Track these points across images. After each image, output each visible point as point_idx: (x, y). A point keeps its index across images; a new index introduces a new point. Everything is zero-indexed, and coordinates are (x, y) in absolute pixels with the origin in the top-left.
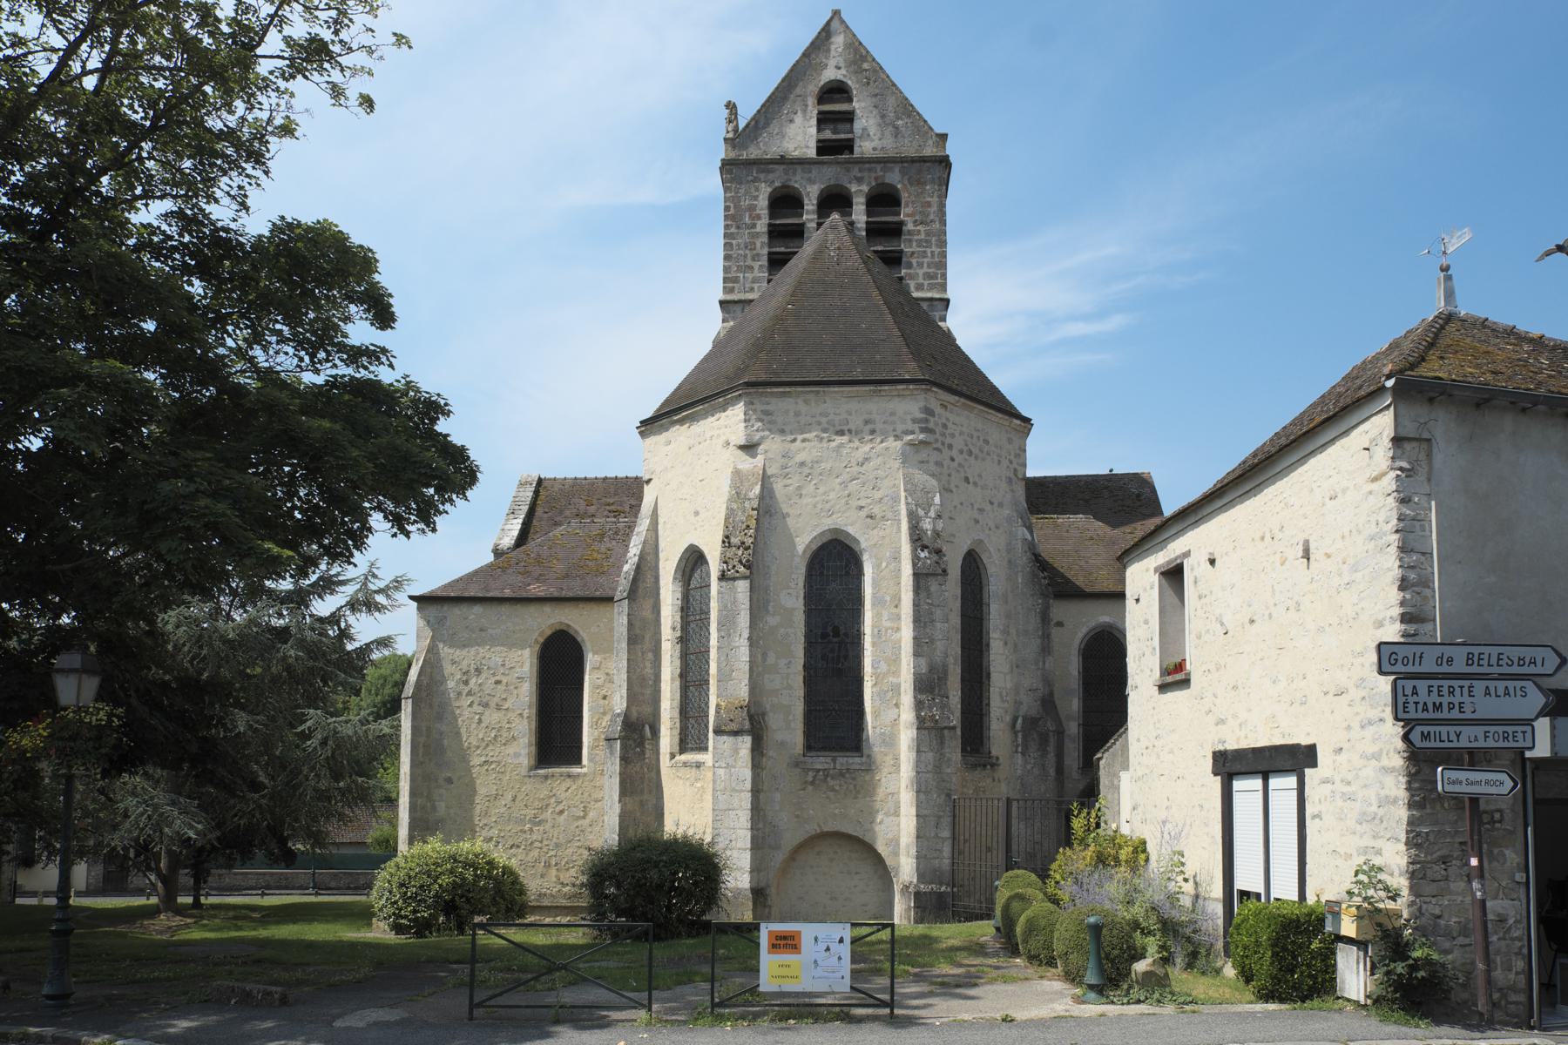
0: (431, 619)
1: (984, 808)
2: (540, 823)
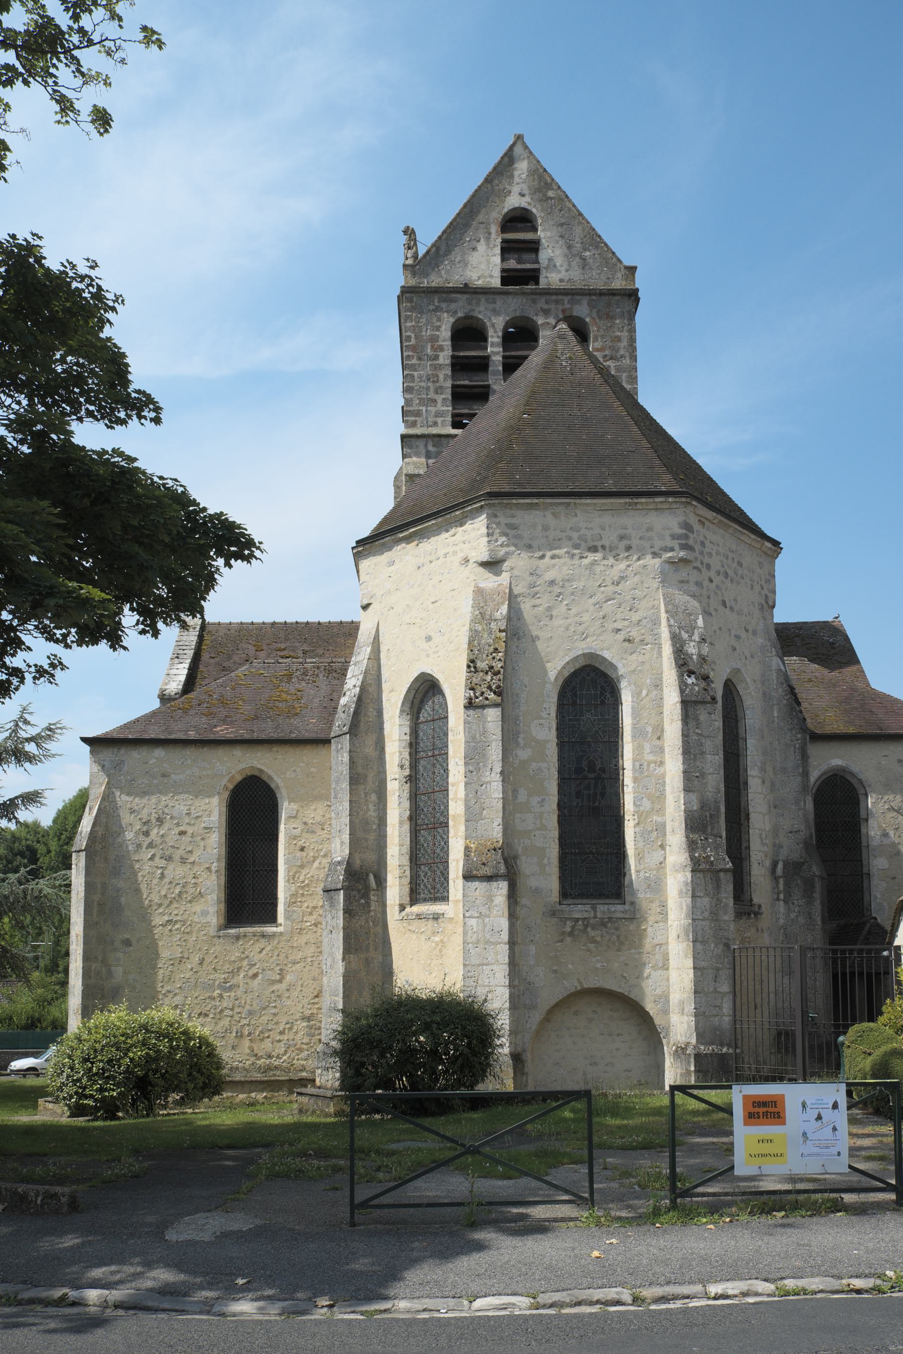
0: (106, 763)
1: (751, 960)
2: (230, 989)
